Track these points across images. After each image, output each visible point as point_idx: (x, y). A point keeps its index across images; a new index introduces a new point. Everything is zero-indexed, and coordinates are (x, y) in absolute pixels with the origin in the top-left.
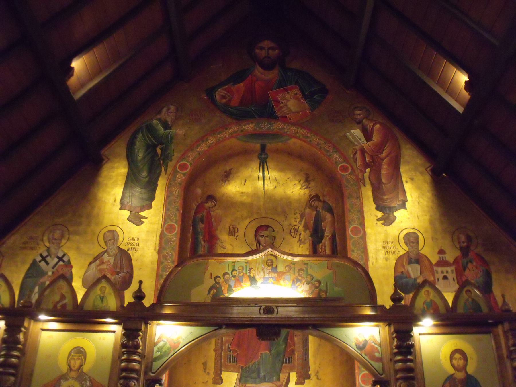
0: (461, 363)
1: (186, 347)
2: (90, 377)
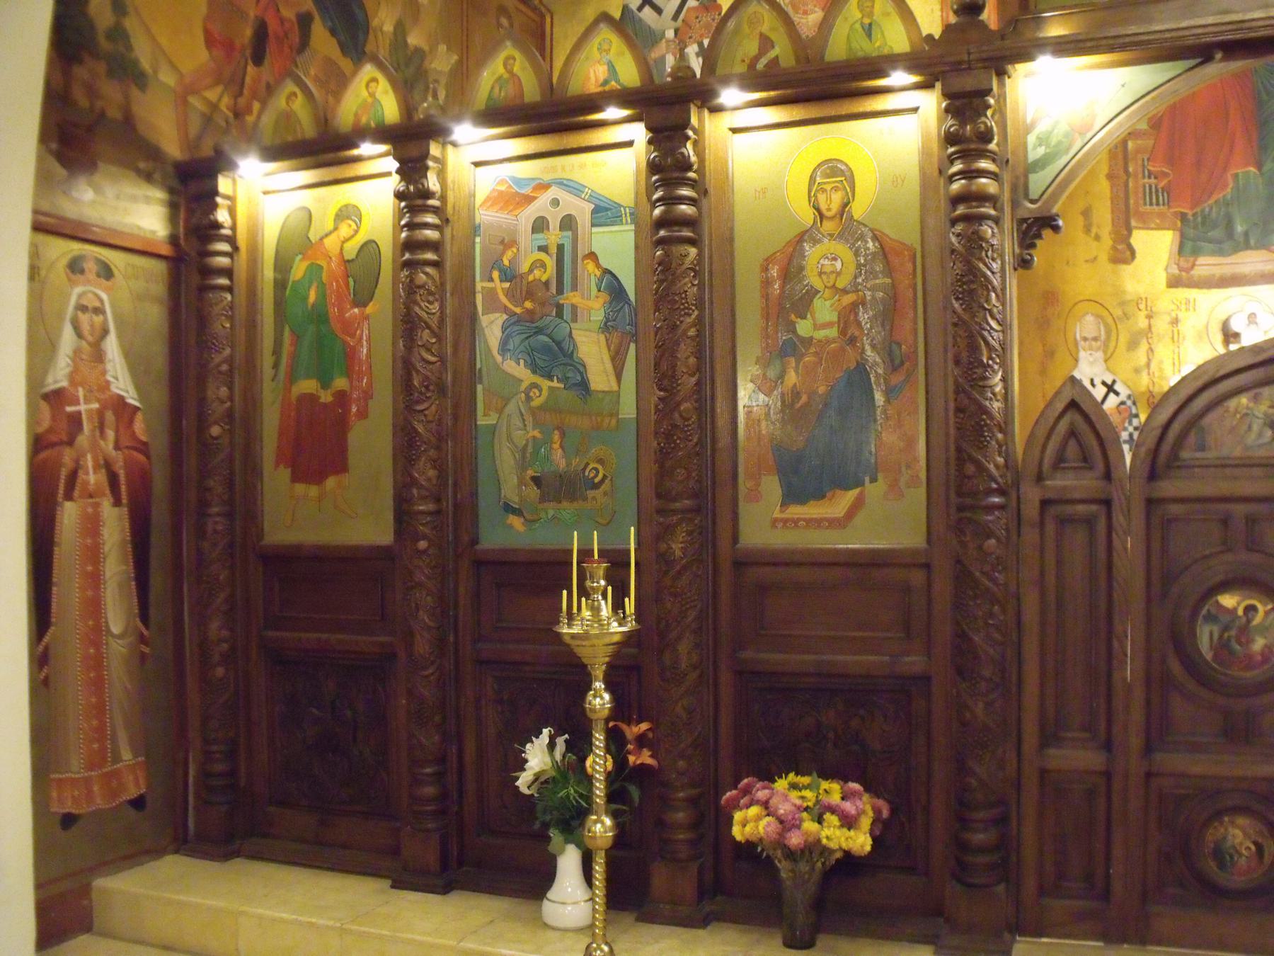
1: (1107, 133)
2: (872, 230)
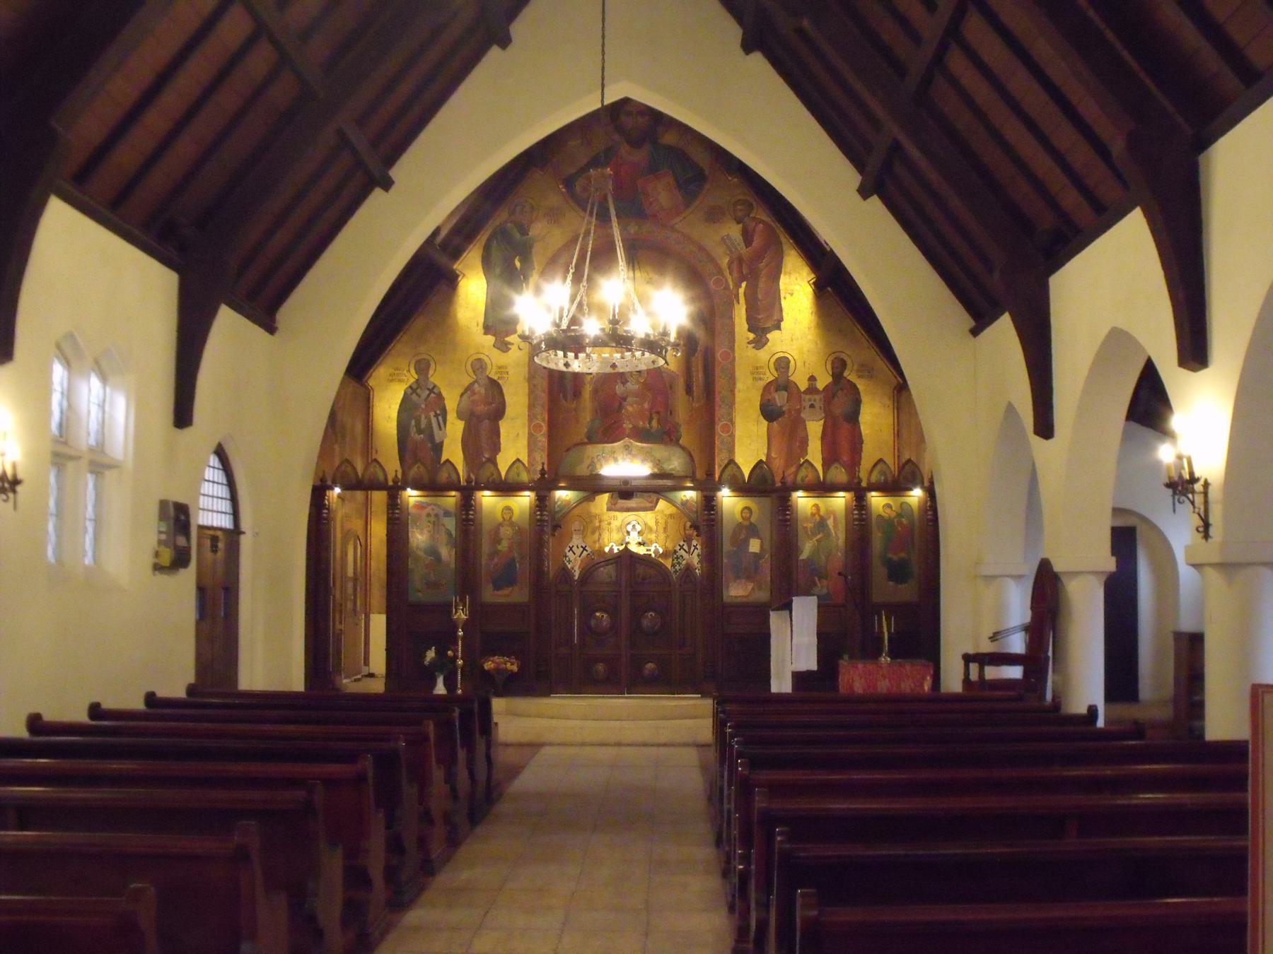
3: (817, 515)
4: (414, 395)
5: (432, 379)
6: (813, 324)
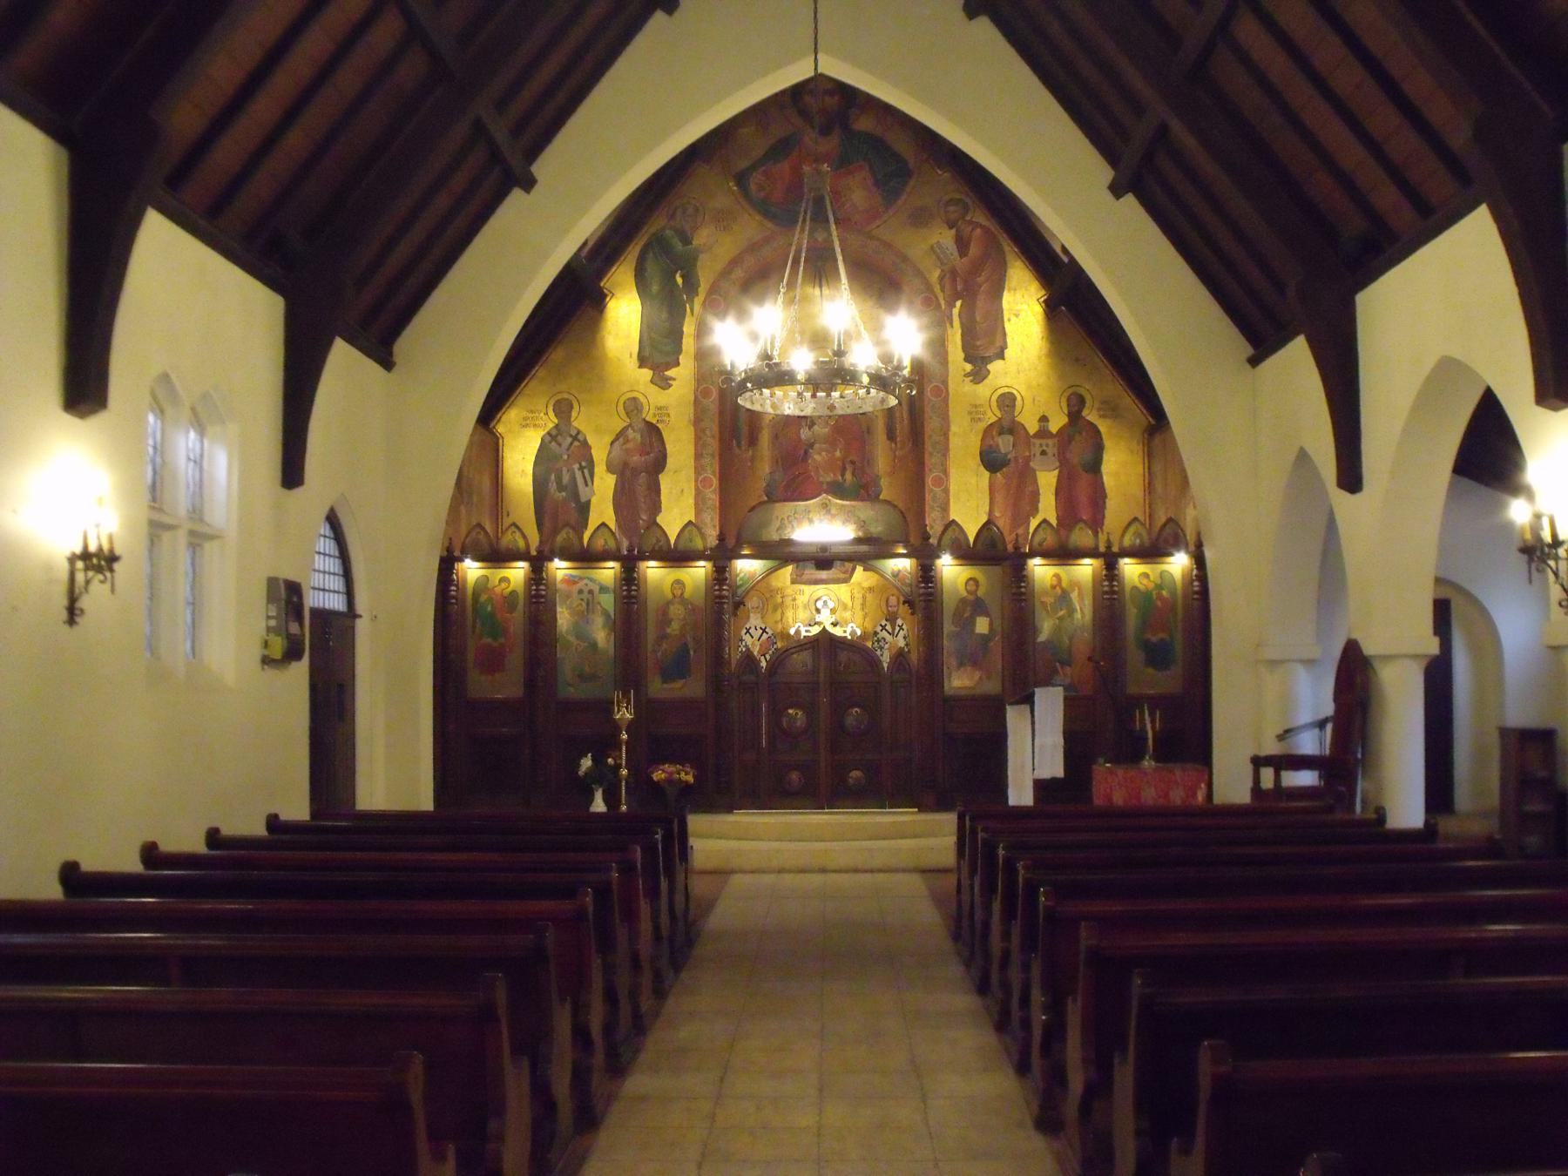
0: (974, 588)
3: (1058, 588)
4: (553, 443)
5: (575, 424)
6: (1044, 351)
